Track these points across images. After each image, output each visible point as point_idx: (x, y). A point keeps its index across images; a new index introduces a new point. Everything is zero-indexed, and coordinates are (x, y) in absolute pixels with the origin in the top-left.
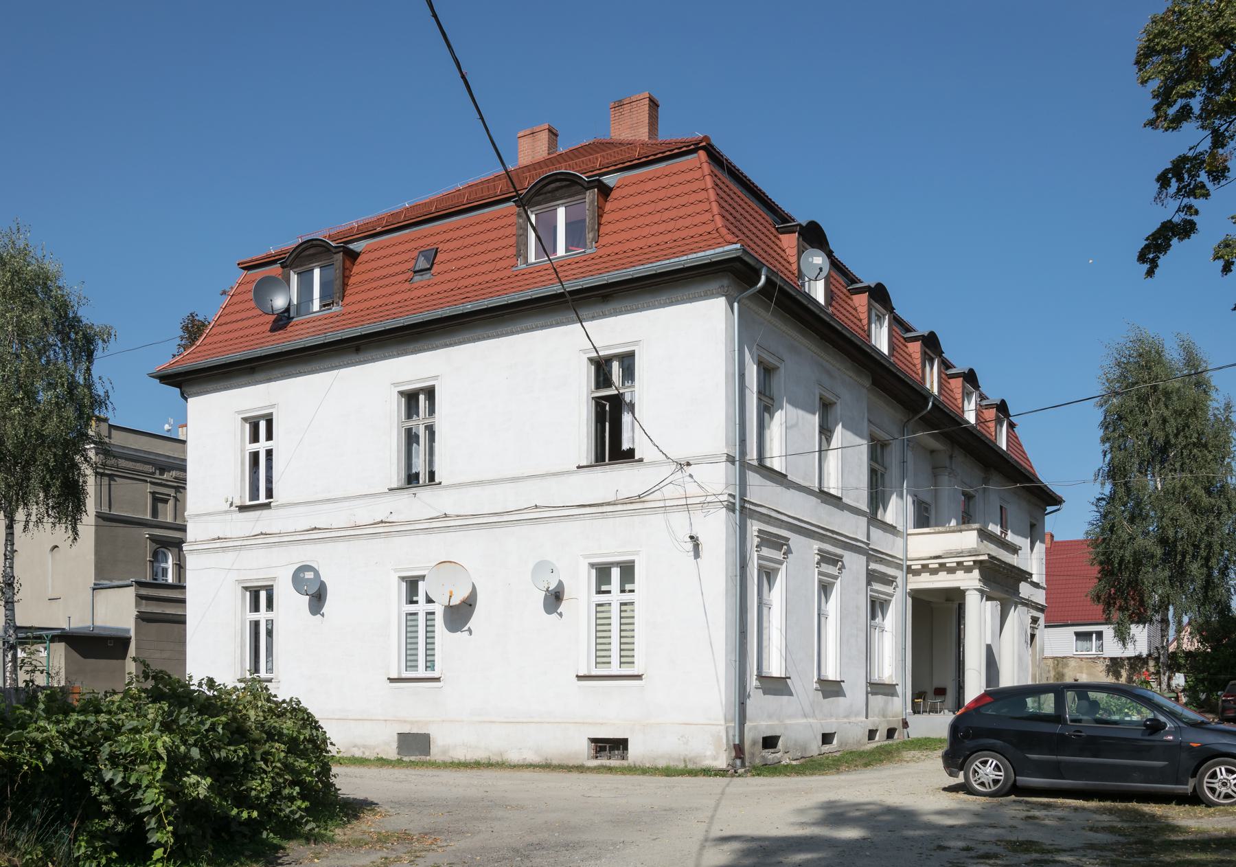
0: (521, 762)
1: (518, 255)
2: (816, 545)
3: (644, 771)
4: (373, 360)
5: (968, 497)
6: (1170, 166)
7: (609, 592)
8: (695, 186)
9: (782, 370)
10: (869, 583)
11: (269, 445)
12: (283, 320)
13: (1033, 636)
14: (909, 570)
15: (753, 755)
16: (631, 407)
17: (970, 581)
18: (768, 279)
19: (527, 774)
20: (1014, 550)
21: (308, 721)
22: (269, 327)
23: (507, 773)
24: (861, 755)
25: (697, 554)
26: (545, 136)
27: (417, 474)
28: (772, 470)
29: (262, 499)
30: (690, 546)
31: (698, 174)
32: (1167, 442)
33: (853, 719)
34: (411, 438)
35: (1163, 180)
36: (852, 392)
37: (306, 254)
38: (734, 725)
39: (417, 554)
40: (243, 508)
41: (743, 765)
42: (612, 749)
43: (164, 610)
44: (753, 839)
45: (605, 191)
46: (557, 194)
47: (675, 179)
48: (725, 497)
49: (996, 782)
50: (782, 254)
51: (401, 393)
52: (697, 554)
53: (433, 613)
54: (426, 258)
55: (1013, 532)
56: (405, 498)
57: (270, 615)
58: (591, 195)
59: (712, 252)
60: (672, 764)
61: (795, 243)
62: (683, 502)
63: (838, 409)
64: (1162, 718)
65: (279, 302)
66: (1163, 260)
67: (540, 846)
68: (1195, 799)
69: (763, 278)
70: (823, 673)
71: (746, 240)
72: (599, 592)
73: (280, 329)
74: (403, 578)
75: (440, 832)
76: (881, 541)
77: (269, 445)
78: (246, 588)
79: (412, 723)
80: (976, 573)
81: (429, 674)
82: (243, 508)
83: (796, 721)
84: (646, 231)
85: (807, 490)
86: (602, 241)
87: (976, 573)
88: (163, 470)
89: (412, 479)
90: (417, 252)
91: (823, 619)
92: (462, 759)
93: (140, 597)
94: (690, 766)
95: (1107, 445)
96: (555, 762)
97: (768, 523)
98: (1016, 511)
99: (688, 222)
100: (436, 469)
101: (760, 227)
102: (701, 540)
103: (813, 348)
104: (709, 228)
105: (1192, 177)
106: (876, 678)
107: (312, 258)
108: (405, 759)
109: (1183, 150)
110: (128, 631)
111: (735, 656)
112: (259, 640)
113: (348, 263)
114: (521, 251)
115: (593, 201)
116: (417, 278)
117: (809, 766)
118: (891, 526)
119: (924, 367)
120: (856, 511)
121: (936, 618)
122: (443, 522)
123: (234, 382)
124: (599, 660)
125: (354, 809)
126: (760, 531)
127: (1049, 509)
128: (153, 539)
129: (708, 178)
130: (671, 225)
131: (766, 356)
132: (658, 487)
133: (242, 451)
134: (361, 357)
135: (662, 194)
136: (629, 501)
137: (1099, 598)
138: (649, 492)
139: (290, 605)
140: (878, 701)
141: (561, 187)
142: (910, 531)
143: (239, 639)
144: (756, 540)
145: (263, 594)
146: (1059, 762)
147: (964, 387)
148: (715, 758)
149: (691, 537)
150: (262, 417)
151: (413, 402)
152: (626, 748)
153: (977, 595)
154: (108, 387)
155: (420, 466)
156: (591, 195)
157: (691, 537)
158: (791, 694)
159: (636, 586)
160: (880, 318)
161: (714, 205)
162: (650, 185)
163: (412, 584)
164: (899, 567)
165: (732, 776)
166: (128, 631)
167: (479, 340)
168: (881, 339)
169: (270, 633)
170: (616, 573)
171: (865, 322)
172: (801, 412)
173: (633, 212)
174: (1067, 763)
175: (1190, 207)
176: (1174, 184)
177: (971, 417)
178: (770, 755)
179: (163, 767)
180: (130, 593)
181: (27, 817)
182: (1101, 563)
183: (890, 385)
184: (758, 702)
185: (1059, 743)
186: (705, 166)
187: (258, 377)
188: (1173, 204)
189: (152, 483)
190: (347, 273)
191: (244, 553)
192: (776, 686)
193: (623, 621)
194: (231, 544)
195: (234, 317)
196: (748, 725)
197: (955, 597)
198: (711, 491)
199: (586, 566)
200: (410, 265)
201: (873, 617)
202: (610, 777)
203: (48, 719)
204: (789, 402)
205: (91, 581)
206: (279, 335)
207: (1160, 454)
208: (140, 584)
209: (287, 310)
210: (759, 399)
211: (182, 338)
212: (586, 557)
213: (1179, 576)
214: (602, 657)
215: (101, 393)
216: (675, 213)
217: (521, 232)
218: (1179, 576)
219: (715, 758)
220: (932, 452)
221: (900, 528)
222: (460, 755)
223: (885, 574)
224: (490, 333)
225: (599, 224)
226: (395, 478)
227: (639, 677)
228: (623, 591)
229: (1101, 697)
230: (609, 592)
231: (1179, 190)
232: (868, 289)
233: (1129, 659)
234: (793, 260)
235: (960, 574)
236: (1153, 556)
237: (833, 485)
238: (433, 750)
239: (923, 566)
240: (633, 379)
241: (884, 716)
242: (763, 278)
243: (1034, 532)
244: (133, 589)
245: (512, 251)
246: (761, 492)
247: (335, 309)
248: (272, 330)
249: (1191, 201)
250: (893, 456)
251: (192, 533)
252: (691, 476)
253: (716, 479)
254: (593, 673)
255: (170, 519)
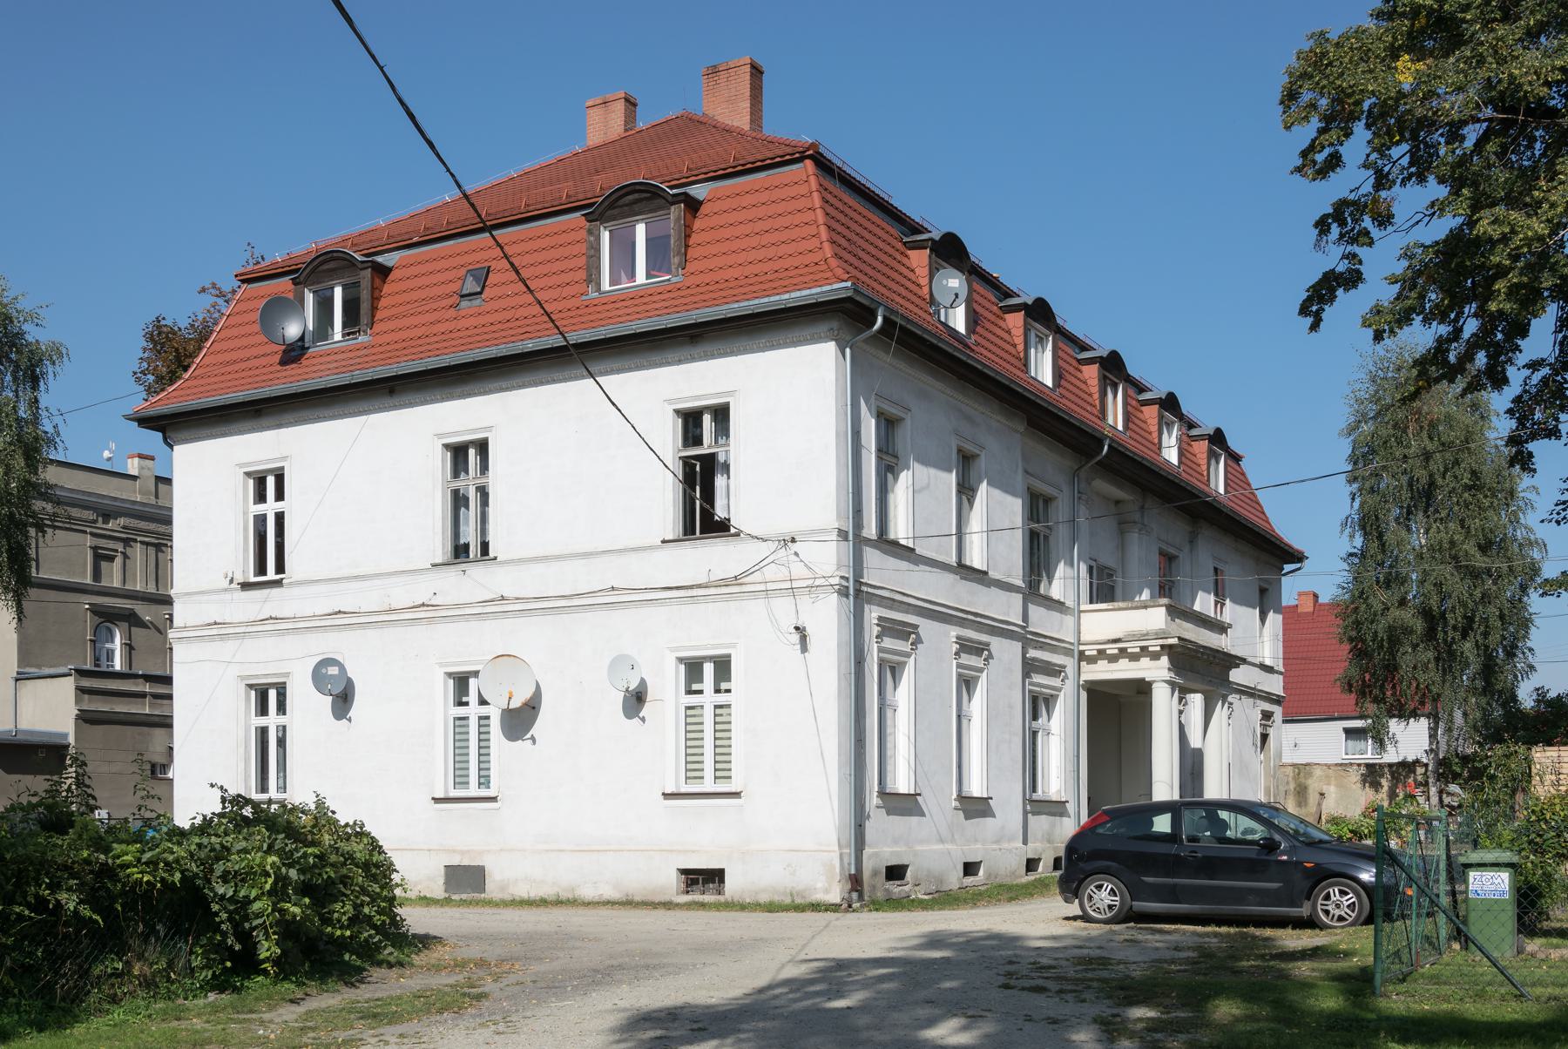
0: (597, 899)
1: (589, 281)
2: (954, 632)
3: (743, 907)
4: (411, 405)
5: (1168, 559)
6: (1331, 211)
7: (701, 692)
8: (801, 204)
9: (908, 422)
10: (1026, 674)
11: (279, 506)
12: (294, 353)
13: (1265, 737)
14: (1082, 656)
15: (874, 887)
16: (726, 468)
17: (1157, 671)
18: (885, 318)
19: (604, 912)
20: (1222, 628)
21: (375, 846)
22: (277, 358)
23: (581, 911)
24: (1010, 888)
25: (804, 649)
26: (620, 106)
27: (467, 546)
28: (895, 543)
29: (271, 575)
30: (796, 637)
31: (803, 190)
32: (1432, 484)
33: (1006, 845)
34: (459, 500)
35: (1322, 225)
36: (1000, 439)
37: (320, 268)
38: (850, 851)
39: (469, 646)
40: (246, 586)
41: (861, 897)
42: (705, 882)
43: (133, 707)
44: (834, 960)
45: (693, 205)
46: (636, 208)
47: (777, 194)
48: (836, 581)
49: (1110, 907)
50: (910, 275)
51: (447, 446)
52: (804, 649)
53: (488, 718)
54: (476, 279)
55: (1234, 601)
56: (452, 575)
57: (282, 720)
58: (677, 211)
59: (818, 290)
60: (776, 898)
61: (926, 261)
62: (788, 585)
63: (982, 463)
64: (1277, 837)
65: (293, 330)
66: (1329, 312)
67: (621, 967)
68: (1311, 923)
69: (880, 320)
70: (965, 789)
71: (859, 275)
72: (689, 692)
73: (293, 362)
74: (450, 675)
75: (517, 959)
76: (1043, 621)
77: (279, 506)
78: (251, 686)
79: (462, 853)
80: (1165, 661)
81: (484, 793)
82: (246, 586)
83: (931, 845)
84: (742, 258)
85: (944, 567)
86: (691, 267)
87: (1165, 660)
88: (107, 517)
89: (460, 552)
90: (463, 271)
91: (964, 722)
92: (525, 896)
93: (81, 691)
94: (798, 901)
95: (1355, 486)
96: (637, 898)
97: (891, 608)
98: (1238, 573)
99: (790, 249)
100: (491, 538)
101: (881, 244)
102: (809, 631)
103: (948, 391)
104: (817, 257)
105: (1356, 221)
106: (1039, 795)
107: (333, 274)
108: (454, 897)
109: (1344, 193)
110: (66, 736)
111: (849, 769)
112: (268, 751)
113: (378, 281)
114: (593, 277)
115: (678, 220)
116: (465, 304)
117: (944, 899)
118: (1058, 602)
119: (1103, 395)
120: (1008, 587)
121: (1116, 716)
122: (499, 606)
123: (234, 427)
124: (690, 774)
125: (425, 941)
126: (880, 618)
127: (1288, 568)
128: (96, 610)
129: (815, 195)
130: (771, 252)
131: (887, 407)
132: (758, 567)
133: (245, 513)
134: (395, 400)
135: (761, 211)
136: (724, 583)
137: (1350, 685)
138: (746, 573)
139: (308, 709)
140: (1039, 823)
141: (640, 200)
142: (1083, 608)
143: (242, 750)
144: (876, 630)
145: (272, 694)
146: (1175, 886)
147: (1161, 417)
148: (827, 891)
149: (797, 628)
150: (270, 471)
151: (461, 459)
152: (722, 881)
153: (1166, 689)
154: (58, 420)
155: (470, 535)
156: (677, 211)
157: (797, 628)
158: (922, 814)
159: (732, 685)
160: (1041, 340)
161: (823, 229)
162: (747, 200)
163: (461, 682)
164: (1068, 652)
165: (846, 911)
166: (66, 736)
167: (542, 384)
168: (1043, 368)
169: (281, 742)
170: (709, 669)
171: (1021, 347)
172: (933, 471)
173: (727, 233)
174: (1184, 886)
175: (1355, 256)
176: (1335, 230)
177: (1171, 455)
178: (895, 888)
179: (270, 881)
180: (68, 685)
181: (153, 931)
182: (1351, 640)
183: (1050, 425)
184: (880, 824)
185: (1173, 865)
186: (812, 179)
187: (265, 421)
188: (1339, 250)
189: (92, 534)
190: (377, 293)
191: (248, 642)
192: (904, 805)
193: (718, 727)
194: (232, 631)
195: (231, 344)
196: (867, 851)
197: (1142, 688)
198: (820, 573)
199: (674, 661)
200: (455, 287)
201: (1035, 717)
202: (701, 914)
203: (170, 841)
204: (918, 460)
205: (13, 668)
206: (292, 369)
207: (1424, 497)
208: (81, 673)
209: (302, 338)
210: (879, 458)
211: (145, 350)
212: (673, 650)
213: (1448, 660)
214: (693, 769)
215: (49, 428)
216: (774, 235)
217: (592, 252)
218: (1448, 660)
219: (827, 891)
220: (1117, 502)
221: (1069, 603)
222: (522, 892)
223: (1048, 663)
224: (556, 375)
225: (687, 246)
226: (439, 552)
227: (736, 795)
228: (717, 691)
229: (1224, 815)
230: (701, 692)
231: (1342, 236)
232: (1024, 307)
233: (1390, 765)
234: (924, 281)
235: (1145, 661)
236: (1412, 632)
237: (976, 558)
238: (489, 885)
239: (1099, 651)
240: (728, 436)
241: (1049, 841)
242: (880, 320)
243: (1265, 599)
244: (71, 680)
245: (582, 275)
246: (882, 571)
247: (362, 338)
248: (283, 363)
249: (1355, 249)
250: (1061, 509)
251: (182, 613)
252: (796, 554)
253: (827, 558)
254: (684, 789)
255: (116, 584)
